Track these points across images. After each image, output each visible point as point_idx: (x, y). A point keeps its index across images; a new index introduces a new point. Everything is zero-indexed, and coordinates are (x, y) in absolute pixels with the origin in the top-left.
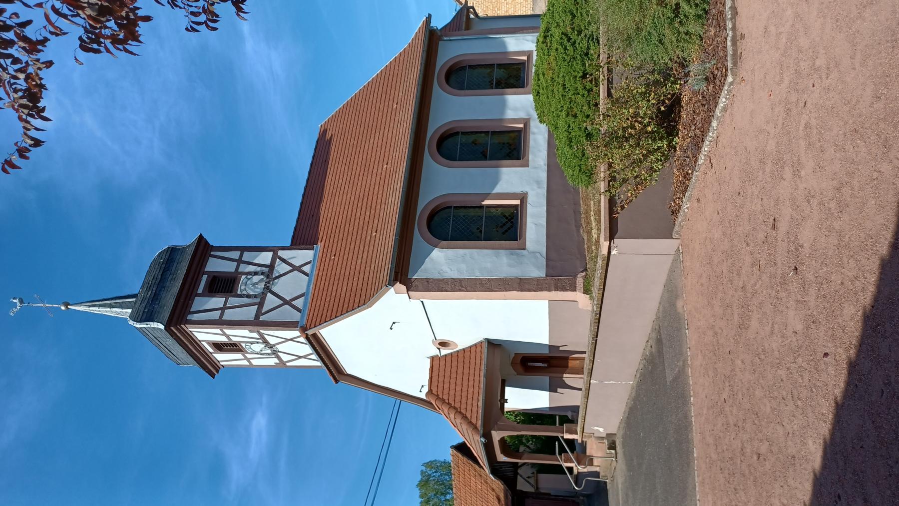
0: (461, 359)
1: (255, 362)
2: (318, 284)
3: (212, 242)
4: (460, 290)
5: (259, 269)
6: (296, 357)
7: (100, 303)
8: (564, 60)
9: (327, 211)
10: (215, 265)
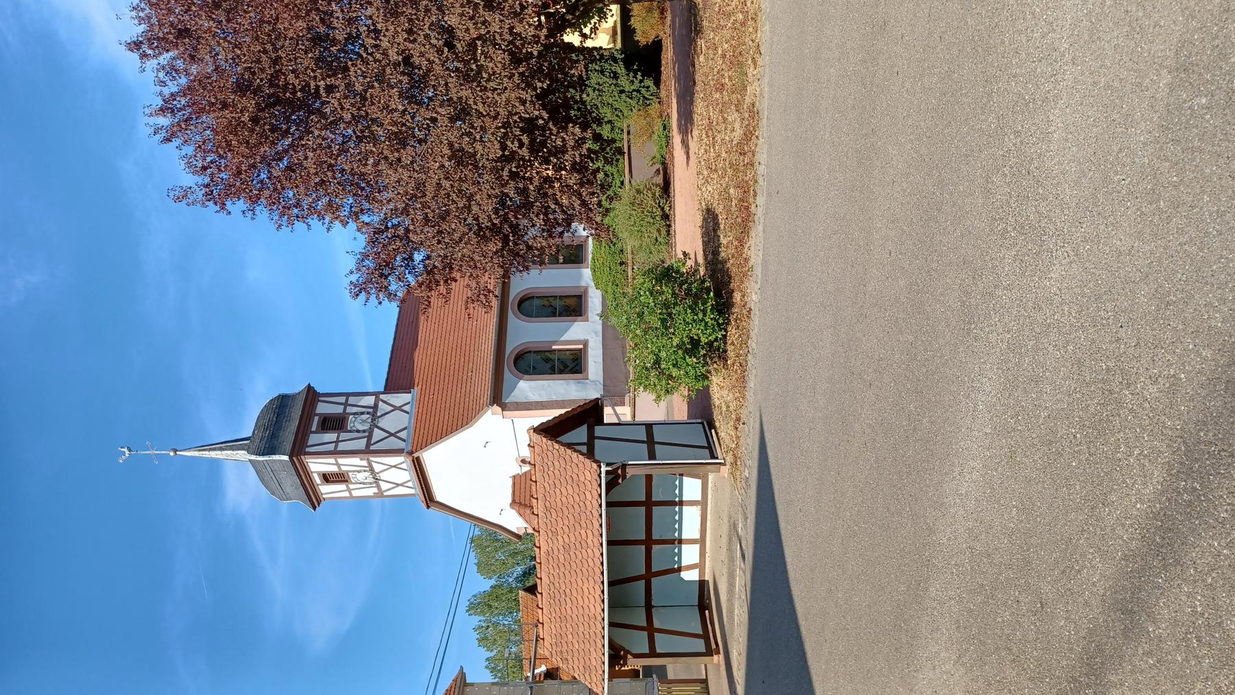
1: (355, 493)
2: (419, 418)
3: (319, 389)
4: (541, 409)
5: (363, 410)
6: (394, 485)
7: (211, 447)
8: (610, 253)
9: (420, 358)
10: (323, 408)
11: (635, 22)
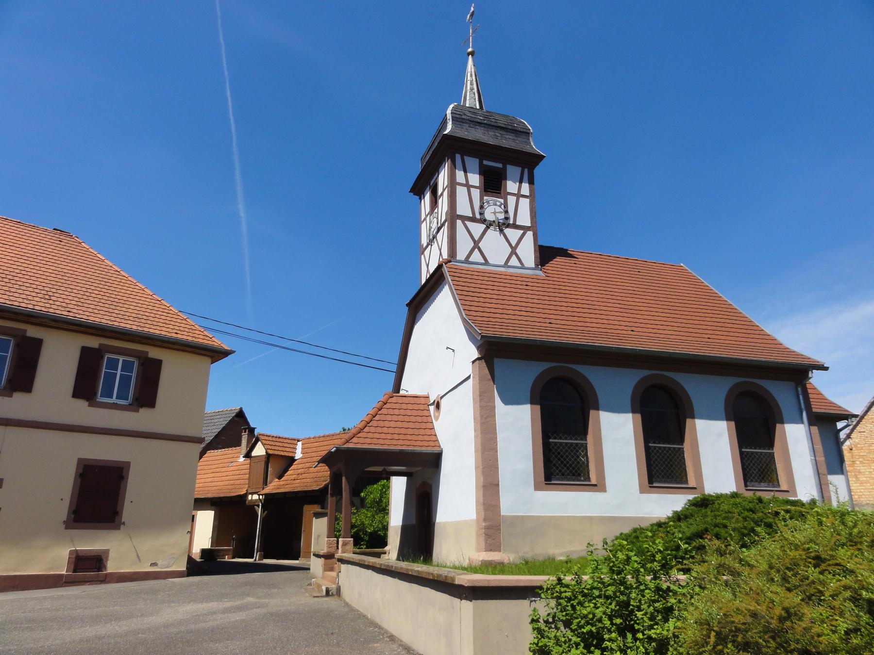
0: (423, 426)
1: (424, 226)
3: (537, 171)
11: (817, 459)
